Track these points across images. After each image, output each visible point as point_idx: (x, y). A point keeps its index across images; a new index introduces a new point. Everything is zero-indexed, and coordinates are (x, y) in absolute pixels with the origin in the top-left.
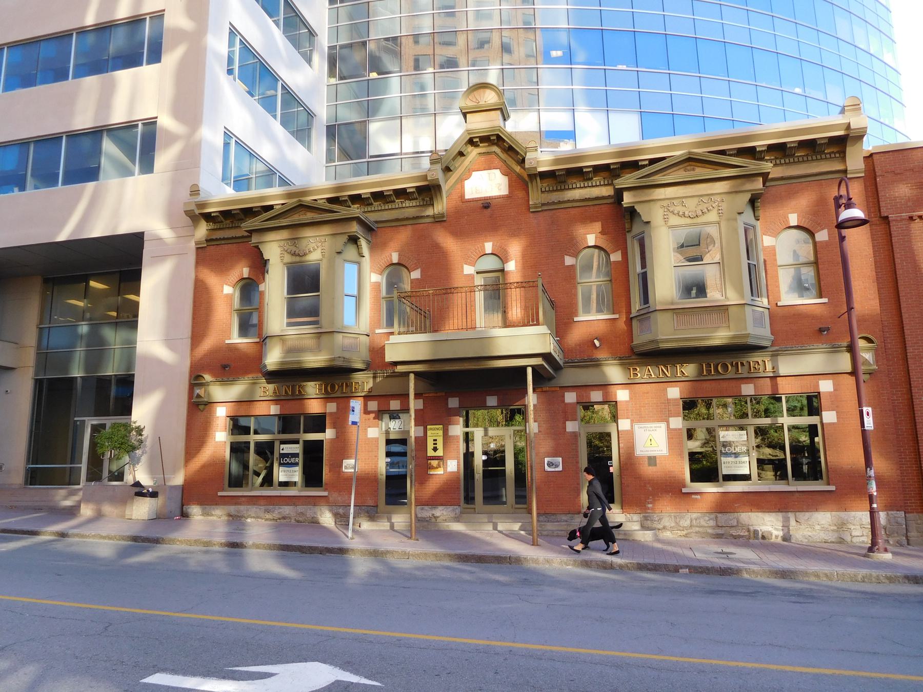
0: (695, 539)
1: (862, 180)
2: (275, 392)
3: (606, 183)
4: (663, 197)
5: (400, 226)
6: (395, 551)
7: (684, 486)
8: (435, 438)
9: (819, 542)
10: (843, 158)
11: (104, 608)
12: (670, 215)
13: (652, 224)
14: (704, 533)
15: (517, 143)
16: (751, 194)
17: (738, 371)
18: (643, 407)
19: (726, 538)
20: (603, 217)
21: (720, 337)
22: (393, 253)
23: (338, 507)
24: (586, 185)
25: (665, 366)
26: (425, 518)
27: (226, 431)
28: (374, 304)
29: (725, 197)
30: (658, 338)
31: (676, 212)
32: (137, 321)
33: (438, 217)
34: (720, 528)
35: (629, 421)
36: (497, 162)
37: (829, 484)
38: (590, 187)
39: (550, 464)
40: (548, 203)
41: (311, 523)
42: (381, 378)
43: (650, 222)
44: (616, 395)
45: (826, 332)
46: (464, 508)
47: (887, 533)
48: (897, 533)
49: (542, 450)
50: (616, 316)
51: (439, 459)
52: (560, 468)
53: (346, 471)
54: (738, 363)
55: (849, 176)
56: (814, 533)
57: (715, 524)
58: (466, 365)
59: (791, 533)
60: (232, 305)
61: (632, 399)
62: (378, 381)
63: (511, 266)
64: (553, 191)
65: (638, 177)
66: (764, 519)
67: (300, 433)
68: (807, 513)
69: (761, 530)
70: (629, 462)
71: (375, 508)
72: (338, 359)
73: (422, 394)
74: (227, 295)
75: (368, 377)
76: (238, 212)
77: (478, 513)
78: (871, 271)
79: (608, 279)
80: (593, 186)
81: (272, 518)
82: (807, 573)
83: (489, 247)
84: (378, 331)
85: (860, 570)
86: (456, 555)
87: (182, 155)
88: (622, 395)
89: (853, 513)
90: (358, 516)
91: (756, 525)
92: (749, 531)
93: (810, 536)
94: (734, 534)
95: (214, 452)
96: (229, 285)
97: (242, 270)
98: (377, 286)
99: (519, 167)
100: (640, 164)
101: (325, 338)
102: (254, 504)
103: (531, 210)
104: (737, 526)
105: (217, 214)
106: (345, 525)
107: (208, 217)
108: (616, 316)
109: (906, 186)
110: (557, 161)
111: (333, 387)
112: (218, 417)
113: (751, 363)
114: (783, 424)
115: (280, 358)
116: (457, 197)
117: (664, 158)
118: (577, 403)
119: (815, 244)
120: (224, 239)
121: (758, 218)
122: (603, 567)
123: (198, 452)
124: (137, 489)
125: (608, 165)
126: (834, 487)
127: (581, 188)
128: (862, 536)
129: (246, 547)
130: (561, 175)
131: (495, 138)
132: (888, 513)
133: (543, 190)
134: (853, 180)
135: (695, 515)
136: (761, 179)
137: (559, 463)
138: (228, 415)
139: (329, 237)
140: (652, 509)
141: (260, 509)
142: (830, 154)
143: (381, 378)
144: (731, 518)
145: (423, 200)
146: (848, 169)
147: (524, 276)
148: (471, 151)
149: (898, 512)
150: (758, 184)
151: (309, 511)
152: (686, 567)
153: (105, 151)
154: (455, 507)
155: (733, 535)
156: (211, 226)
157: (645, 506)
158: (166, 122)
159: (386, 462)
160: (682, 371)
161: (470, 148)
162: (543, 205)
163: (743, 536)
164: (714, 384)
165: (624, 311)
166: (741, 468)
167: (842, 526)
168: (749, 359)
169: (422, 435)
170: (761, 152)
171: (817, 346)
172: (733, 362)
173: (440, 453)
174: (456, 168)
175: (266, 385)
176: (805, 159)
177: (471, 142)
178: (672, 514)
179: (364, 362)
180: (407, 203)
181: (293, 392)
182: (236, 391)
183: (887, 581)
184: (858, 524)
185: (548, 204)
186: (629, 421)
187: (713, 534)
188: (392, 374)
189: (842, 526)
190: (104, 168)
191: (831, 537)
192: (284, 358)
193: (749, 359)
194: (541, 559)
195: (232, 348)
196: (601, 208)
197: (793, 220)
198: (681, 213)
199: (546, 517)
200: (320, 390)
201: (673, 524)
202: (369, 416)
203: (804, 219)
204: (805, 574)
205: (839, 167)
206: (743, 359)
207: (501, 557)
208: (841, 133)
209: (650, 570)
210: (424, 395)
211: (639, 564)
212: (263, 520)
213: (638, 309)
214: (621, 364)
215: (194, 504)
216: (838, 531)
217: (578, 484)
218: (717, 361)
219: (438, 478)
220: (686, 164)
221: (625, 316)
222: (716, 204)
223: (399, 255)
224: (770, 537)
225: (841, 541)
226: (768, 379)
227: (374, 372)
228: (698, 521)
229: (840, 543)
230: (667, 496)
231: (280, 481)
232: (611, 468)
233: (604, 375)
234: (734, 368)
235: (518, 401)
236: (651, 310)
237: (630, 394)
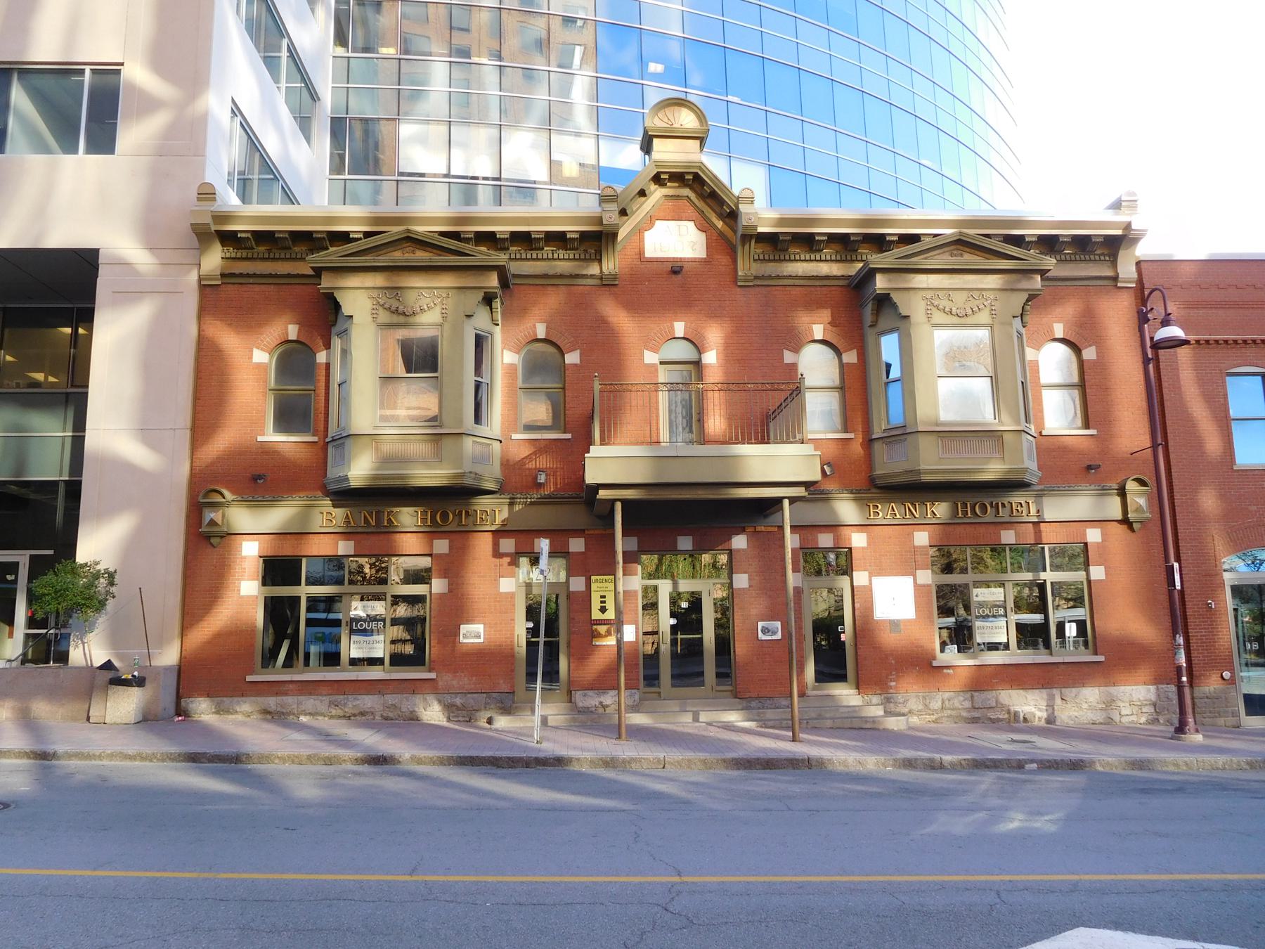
0: (947, 725)
1: (1132, 290)
2: (347, 522)
3: (582, 257)
4: (924, 286)
5: (548, 285)
6: (644, 759)
7: (934, 658)
8: (603, 594)
9: (1087, 724)
10: (1114, 263)
11: (1171, 876)
12: (934, 310)
13: (913, 320)
14: (957, 717)
15: (723, 188)
16: (1029, 294)
17: (998, 514)
18: (883, 556)
19: (983, 723)
20: (832, 302)
21: (993, 470)
22: (537, 324)
23: (453, 696)
24: (529, 256)
25: (912, 504)
26: (588, 708)
27: (258, 580)
28: (509, 397)
29: (999, 295)
30: (921, 468)
31: (941, 307)
32: (87, 393)
33: (608, 279)
34: (976, 710)
35: (866, 573)
36: (690, 211)
37: (1096, 653)
38: (818, 261)
39: (765, 630)
40: (763, 276)
41: (408, 720)
42: (521, 506)
43: (909, 316)
44: (850, 539)
45: (1093, 471)
46: (644, 693)
47: (1158, 710)
48: (1168, 710)
49: (754, 612)
50: (851, 436)
51: (608, 624)
52: (778, 636)
53: (465, 641)
54: (998, 503)
55: (1119, 285)
56: (1081, 713)
57: (970, 706)
58: (700, 492)
59: (1056, 713)
60: (266, 382)
61: (870, 545)
62: (517, 509)
63: (711, 358)
64: (769, 261)
65: (346, 253)
66: (1026, 698)
67: (300, 585)
68: (1074, 690)
69: (1022, 711)
70: (865, 627)
71: (511, 695)
72: (469, 475)
73: (584, 530)
74: (259, 365)
75: (502, 504)
76: (287, 236)
77: (664, 699)
78: (1141, 400)
79: (560, 386)
80: (821, 261)
81: (342, 714)
82: (1165, 762)
83: (679, 328)
84: (514, 436)
85: (1188, 755)
86: (733, 759)
87: (170, 133)
88: (858, 540)
89: (1122, 688)
90: (486, 707)
91: (1017, 705)
92: (1009, 712)
93: (1076, 717)
94: (991, 717)
95: (237, 612)
96: (262, 349)
97: (287, 329)
98: (511, 369)
99: (721, 223)
100: (351, 236)
101: (447, 442)
102: (310, 694)
103: (739, 284)
104: (996, 707)
105: (249, 235)
106: (464, 721)
107: (229, 239)
108: (851, 436)
109: (1174, 303)
110: (782, 221)
111: (445, 516)
112: (245, 557)
113: (1013, 504)
114: (1045, 581)
115: (372, 470)
116: (634, 253)
117: (385, 232)
118: (801, 548)
119: (1081, 364)
120: (254, 275)
121: (497, 322)
122: (931, 766)
123: (207, 613)
124: (110, 675)
125: (847, 235)
126: (1103, 657)
127: (805, 260)
128: (1131, 715)
129: (400, 762)
130: (573, 239)
131: (690, 177)
132: (1157, 687)
133: (756, 257)
134: (1124, 290)
135: (947, 695)
136: (1039, 276)
137: (777, 628)
138: (261, 555)
139: (454, 291)
140: (896, 687)
141: (321, 701)
142: (1099, 255)
143: (521, 506)
144: (990, 697)
145: (586, 251)
146: (1120, 276)
147: (726, 373)
148: (655, 191)
149: (1169, 686)
150: (493, 281)
151: (406, 703)
152: (1032, 761)
153: (15, 106)
154: (633, 691)
155: (991, 718)
156: (231, 252)
157: (886, 684)
158: (137, 74)
159: (527, 629)
160: (933, 511)
161: (653, 187)
162: (756, 278)
163: (1001, 720)
164: (968, 528)
165: (861, 429)
166: (996, 635)
167: (1109, 703)
168: (1011, 500)
169: (583, 589)
170: (504, 239)
171: (1059, 487)
172: (992, 503)
173: (610, 615)
174: (634, 213)
175: (331, 509)
176: (1073, 257)
177: (657, 179)
178: (920, 694)
179: (497, 482)
180: (561, 253)
181: (379, 521)
182: (277, 517)
183: (1248, 767)
184: (1128, 700)
185: (763, 277)
186: (866, 573)
187: (968, 718)
188: (538, 500)
189: (1109, 703)
190: (12, 134)
191: (1099, 717)
192: (378, 469)
193: (1011, 500)
194: (407, 755)
195: (267, 451)
196: (830, 291)
197: (1059, 331)
198: (947, 309)
199: (760, 702)
200: (424, 520)
201: (921, 707)
202: (501, 560)
203: (1070, 332)
204: (1165, 763)
205: (1110, 273)
206: (1005, 499)
207: (797, 760)
208: (1119, 232)
209: (988, 768)
210: (586, 532)
211: (974, 760)
212: (326, 718)
213: (884, 428)
214: (855, 500)
215: (201, 696)
216: (1106, 710)
217: (803, 657)
218: (975, 500)
219: (608, 651)
220: (952, 247)
221: (861, 436)
222: (989, 302)
223: (547, 328)
224: (1033, 720)
225: (1109, 721)
226: (1031, 524)
227: (511, 495)
228: (951, 702)
229: (1108, 724)
230: (914, 671)
231: (351, 657)
232: (842, 636)
233: (834, 513)
234: (994, 509)
235: (721, 544)
236: (908, 431)
237: (868, 538)
